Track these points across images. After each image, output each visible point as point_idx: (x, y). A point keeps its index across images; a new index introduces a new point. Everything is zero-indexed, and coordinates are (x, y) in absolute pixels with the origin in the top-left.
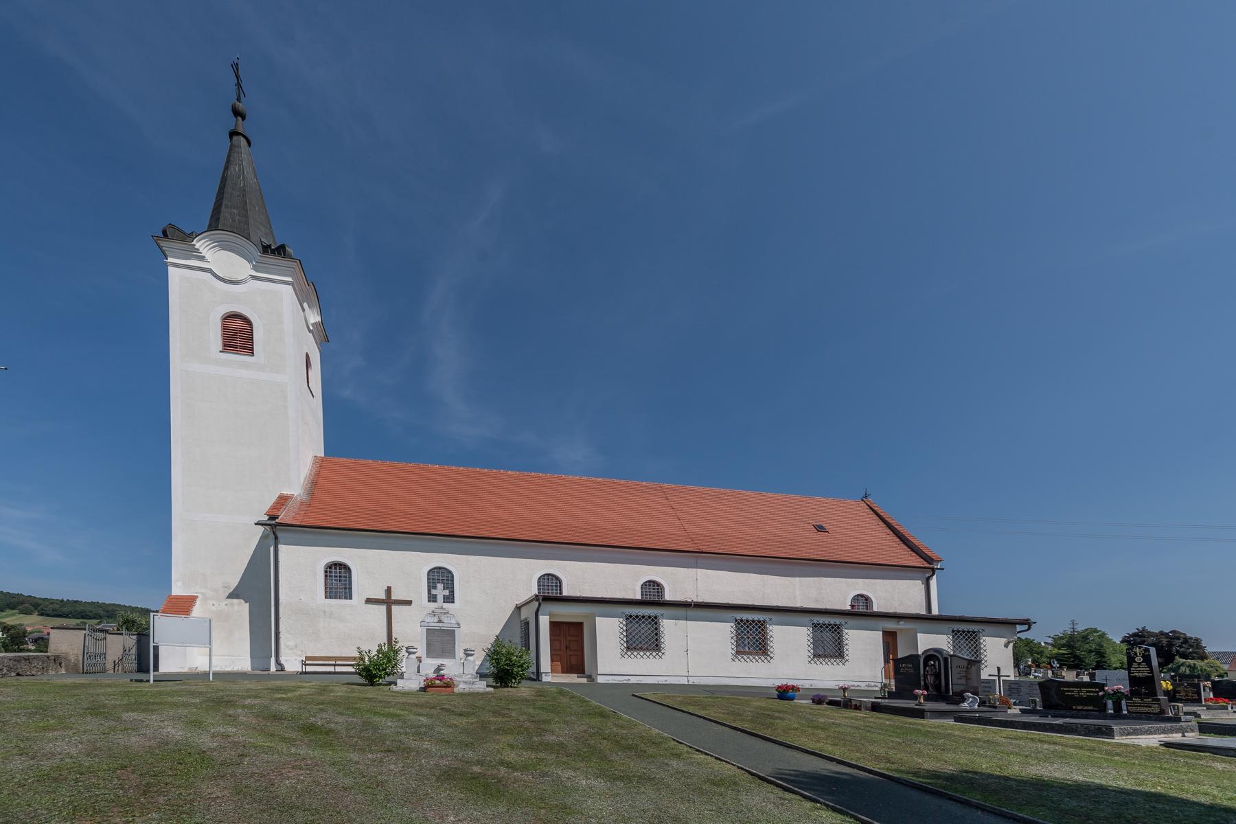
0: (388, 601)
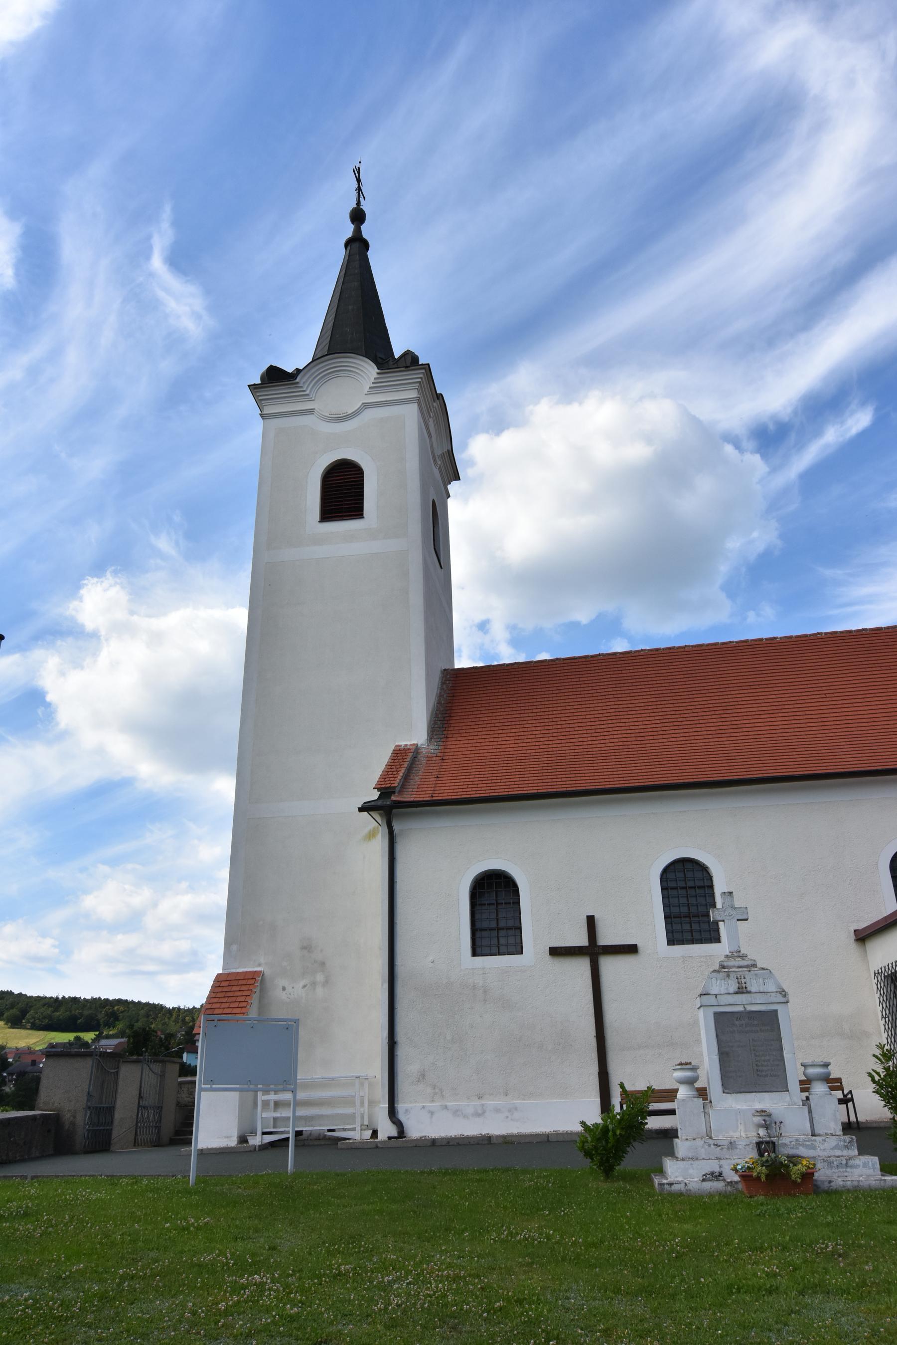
0: (594, 951)
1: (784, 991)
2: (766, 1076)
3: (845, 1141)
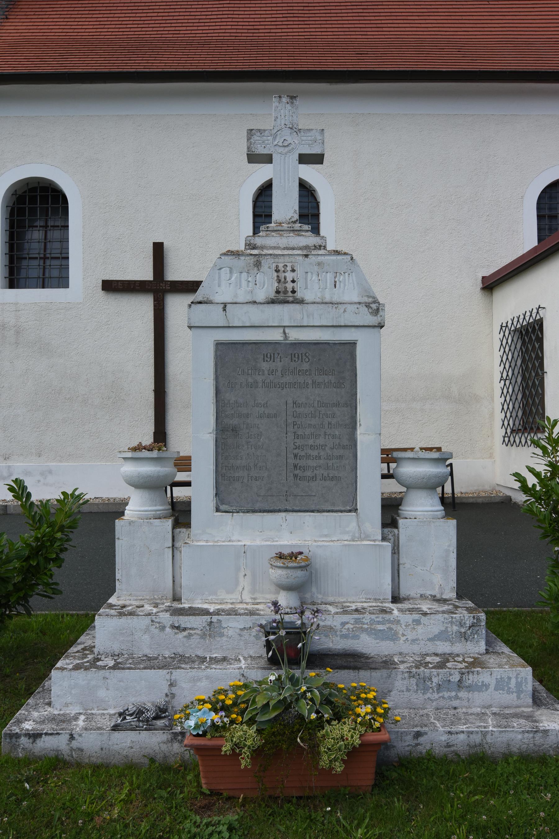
0: (159, 287)
1: (376, 301)
2: (314, 478)
3: (461, 625)
